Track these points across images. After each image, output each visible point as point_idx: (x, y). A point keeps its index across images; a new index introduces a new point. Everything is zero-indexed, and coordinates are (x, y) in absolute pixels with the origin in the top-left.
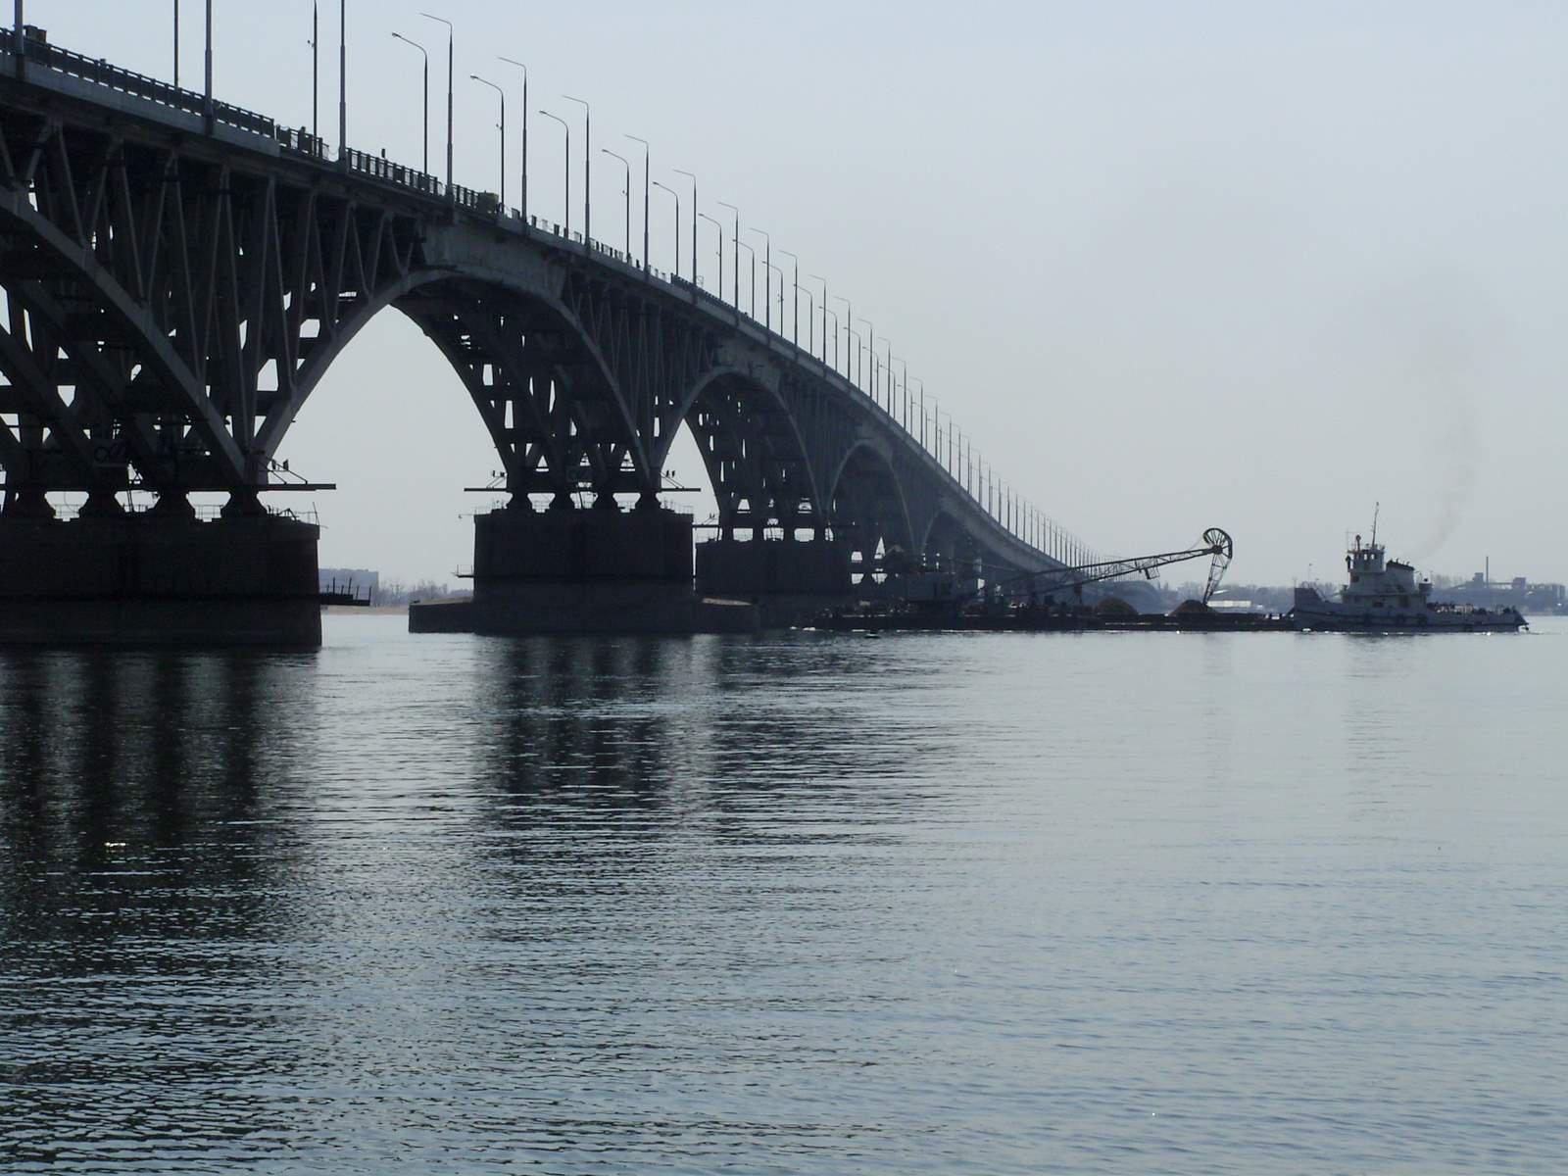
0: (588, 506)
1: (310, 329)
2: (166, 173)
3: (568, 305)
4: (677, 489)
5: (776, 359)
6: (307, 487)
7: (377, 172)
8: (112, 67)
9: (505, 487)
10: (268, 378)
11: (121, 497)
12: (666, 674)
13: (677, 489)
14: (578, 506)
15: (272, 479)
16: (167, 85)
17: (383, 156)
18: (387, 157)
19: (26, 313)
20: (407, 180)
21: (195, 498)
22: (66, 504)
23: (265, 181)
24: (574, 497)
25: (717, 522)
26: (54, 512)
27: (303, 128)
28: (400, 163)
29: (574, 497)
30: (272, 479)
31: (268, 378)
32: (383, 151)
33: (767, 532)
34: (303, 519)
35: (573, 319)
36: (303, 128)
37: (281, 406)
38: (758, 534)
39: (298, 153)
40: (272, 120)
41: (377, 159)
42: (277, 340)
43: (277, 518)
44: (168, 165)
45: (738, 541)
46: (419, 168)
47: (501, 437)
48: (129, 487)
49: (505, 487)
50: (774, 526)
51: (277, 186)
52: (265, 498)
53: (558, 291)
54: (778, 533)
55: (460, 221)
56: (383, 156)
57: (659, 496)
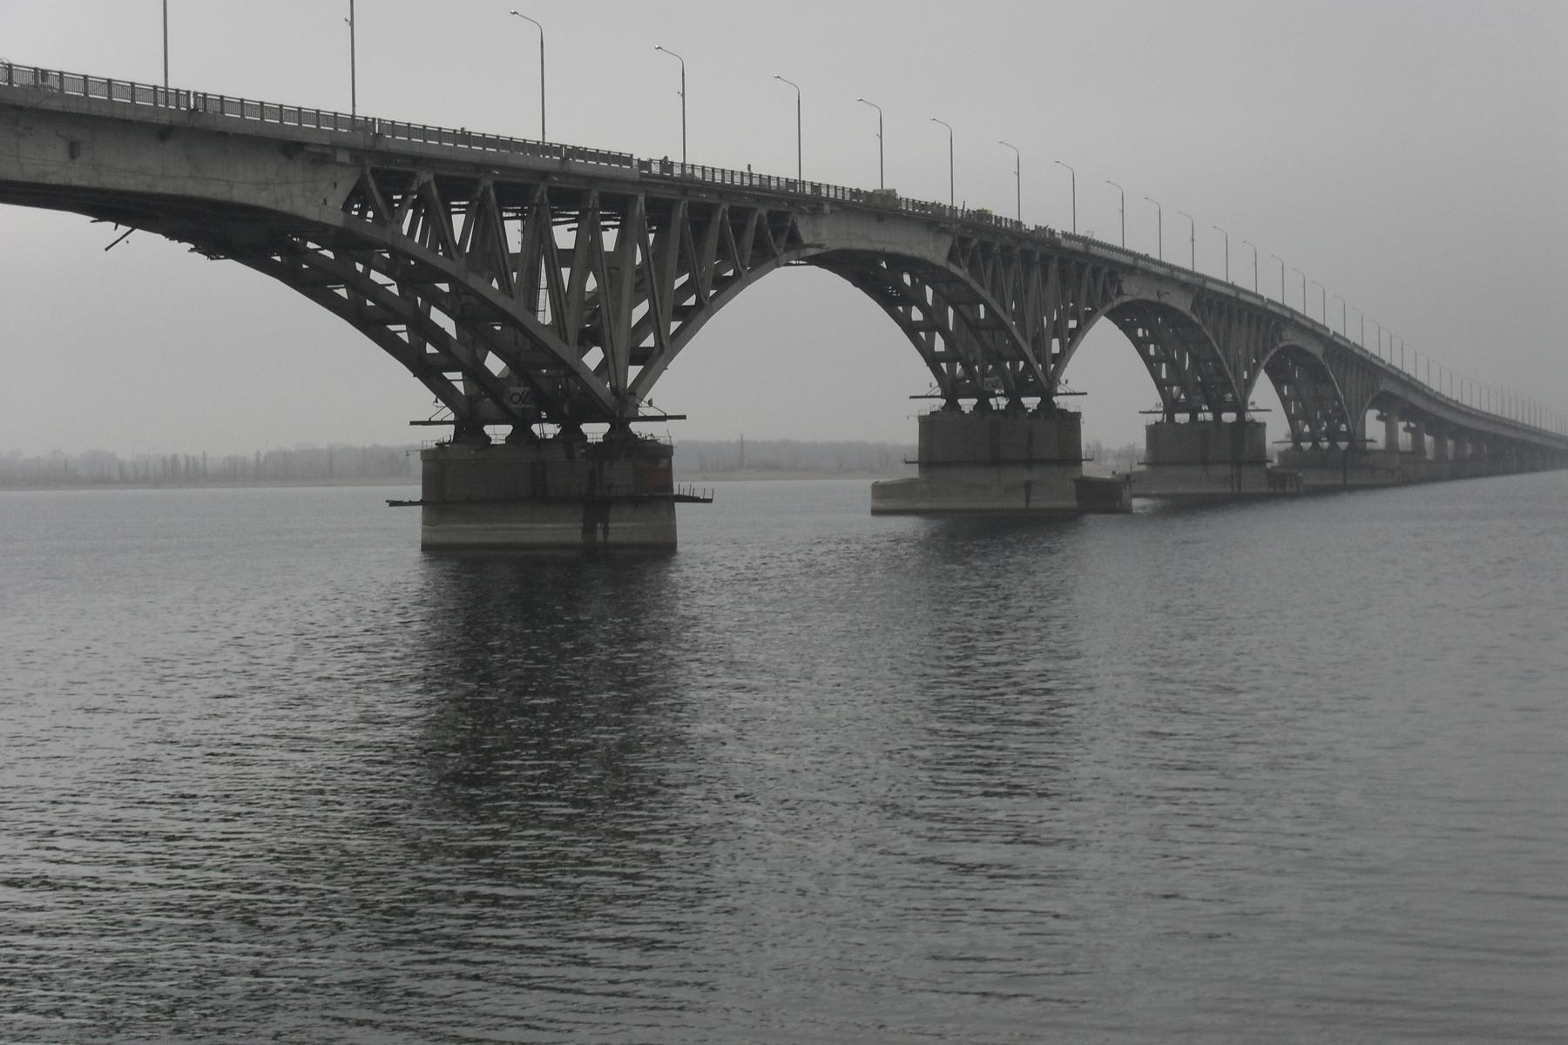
0: (1002, 407)
1: (1072, 324)
2: (536, 200)
3: (958, 264)
4: (1071, 394)
5: (1185, 286)
6: (664, 418)
7: (836, 196)
8: (470, 133)
9: (939, 394)
10: (1055, 346)
11: (536, 428)
12: (370, 719)
13: (1071, 394)
14: (995, 408)
15: (1059, 391)
16: (538, 142)
17: (749, 169)
18: (753, 170)
19: (951, 328)
20: (1003, 224)
21: (586, 428)
22: (498, 433)
23: (635, 197)
24: (992, 401)
25: (1162, 409)
26: (490, 439)
27: (666, 158)
28: (999, 215)
29: (992, 401)
30: (1059, 391)
31: (1055, 346)
32: (749, 166)
33: (1200, 416)
34: (662, 441)
35: (962, 273)
36: (666, 158)
37: (1061, 360)
38: (1193, 418)
39: (661, 177)
40: (632, 155)
41: (742, 174)
42: (934, 322)
43: (644, 441)
44: (538, 194)
45: (1179, 424)
46: (1015, 218)
47: (932, 360)
48: (541, 421)
49: (939, 394)
50: (1205, 411)
51: (646, 200)
52: (635, 427)
53: (945, 254)
54: (1209, 416)
55: (832, 211)
56: (749, 169)
57: (1055, 399)
